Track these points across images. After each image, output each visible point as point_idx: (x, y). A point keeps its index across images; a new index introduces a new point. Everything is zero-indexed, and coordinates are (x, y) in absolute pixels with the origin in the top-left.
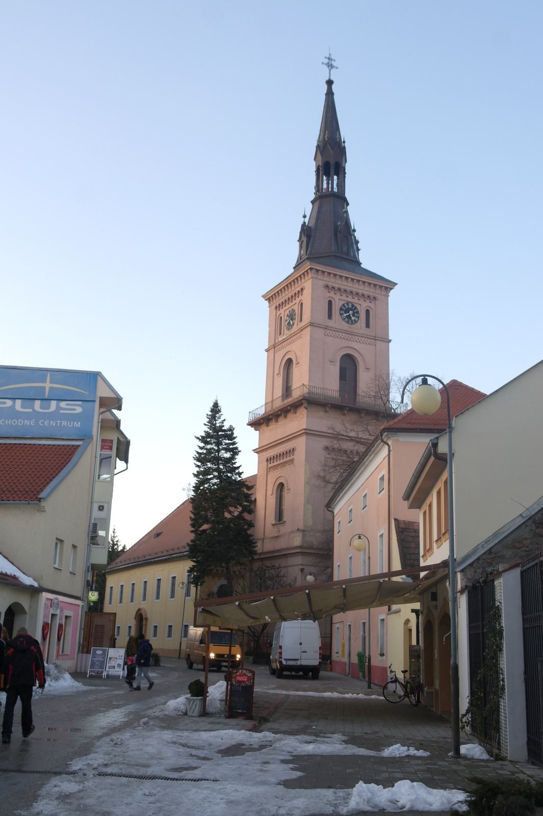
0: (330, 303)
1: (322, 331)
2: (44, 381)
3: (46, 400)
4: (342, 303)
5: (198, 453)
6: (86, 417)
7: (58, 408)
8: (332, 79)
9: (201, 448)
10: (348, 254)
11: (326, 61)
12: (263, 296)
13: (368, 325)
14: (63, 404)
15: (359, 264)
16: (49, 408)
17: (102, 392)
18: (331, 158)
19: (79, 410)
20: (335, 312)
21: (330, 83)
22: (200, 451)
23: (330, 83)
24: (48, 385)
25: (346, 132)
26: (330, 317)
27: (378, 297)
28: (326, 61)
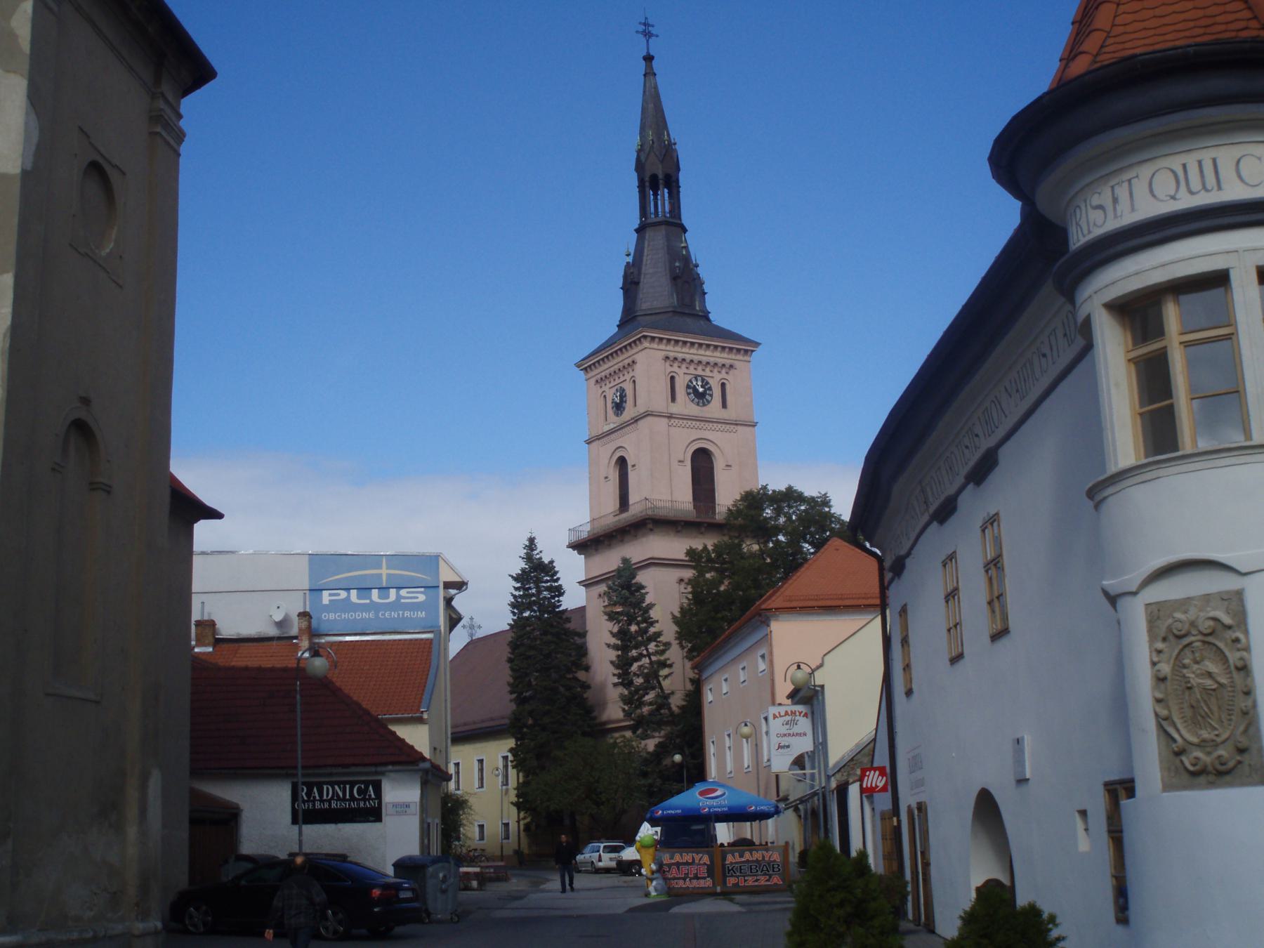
0: (672, 378)
1: (666, 420)
2: (380, 567)
3: (384, 590)
4: (688, 377)
5: (515, 597)
6: (428, 606)
7: (399, 597)
8: (652, 53)
9: (516, 589)
10: (692, 306)
11: (642, 28)
12: (578, 365)
13: (724, 405)
14: (403, 592)
15: (705, 316)
16: (388, 597)
17: (446, 575)
18: (658, 175)
19: (422, 598)
20: (766, 903)
21: (649, 59)
22: (517, 593)
23: (649, 59)
24: (384, 572)
25: (677, 131)
26: (673, 399)
27: (737, 364)
28: (642, 28)
